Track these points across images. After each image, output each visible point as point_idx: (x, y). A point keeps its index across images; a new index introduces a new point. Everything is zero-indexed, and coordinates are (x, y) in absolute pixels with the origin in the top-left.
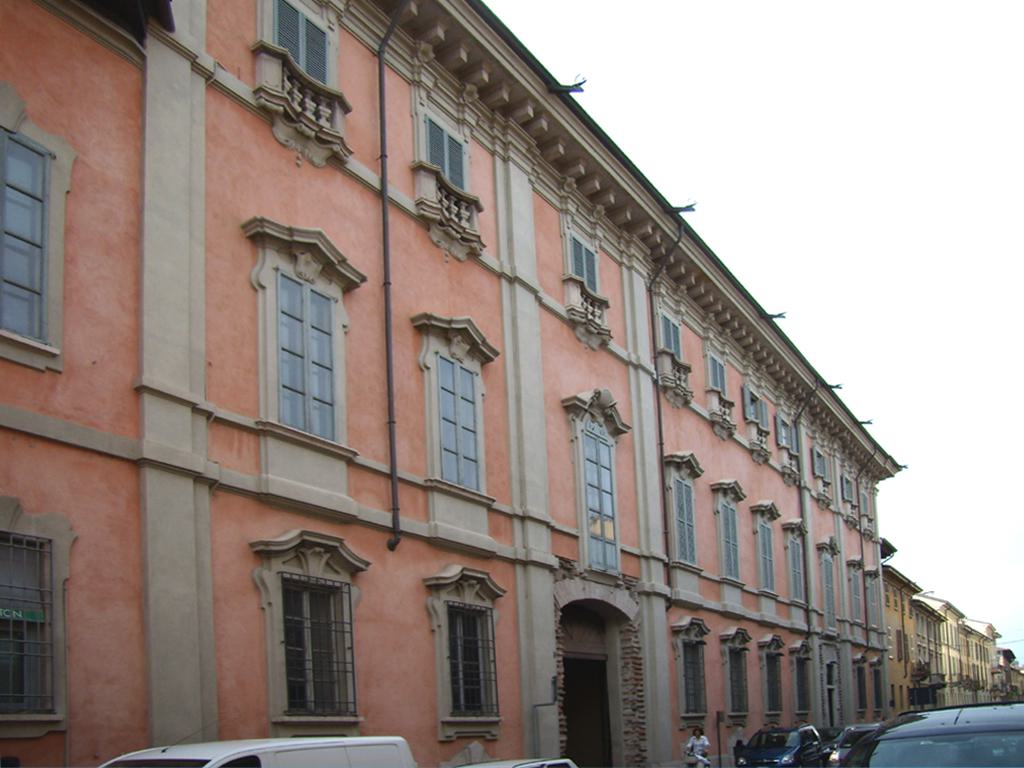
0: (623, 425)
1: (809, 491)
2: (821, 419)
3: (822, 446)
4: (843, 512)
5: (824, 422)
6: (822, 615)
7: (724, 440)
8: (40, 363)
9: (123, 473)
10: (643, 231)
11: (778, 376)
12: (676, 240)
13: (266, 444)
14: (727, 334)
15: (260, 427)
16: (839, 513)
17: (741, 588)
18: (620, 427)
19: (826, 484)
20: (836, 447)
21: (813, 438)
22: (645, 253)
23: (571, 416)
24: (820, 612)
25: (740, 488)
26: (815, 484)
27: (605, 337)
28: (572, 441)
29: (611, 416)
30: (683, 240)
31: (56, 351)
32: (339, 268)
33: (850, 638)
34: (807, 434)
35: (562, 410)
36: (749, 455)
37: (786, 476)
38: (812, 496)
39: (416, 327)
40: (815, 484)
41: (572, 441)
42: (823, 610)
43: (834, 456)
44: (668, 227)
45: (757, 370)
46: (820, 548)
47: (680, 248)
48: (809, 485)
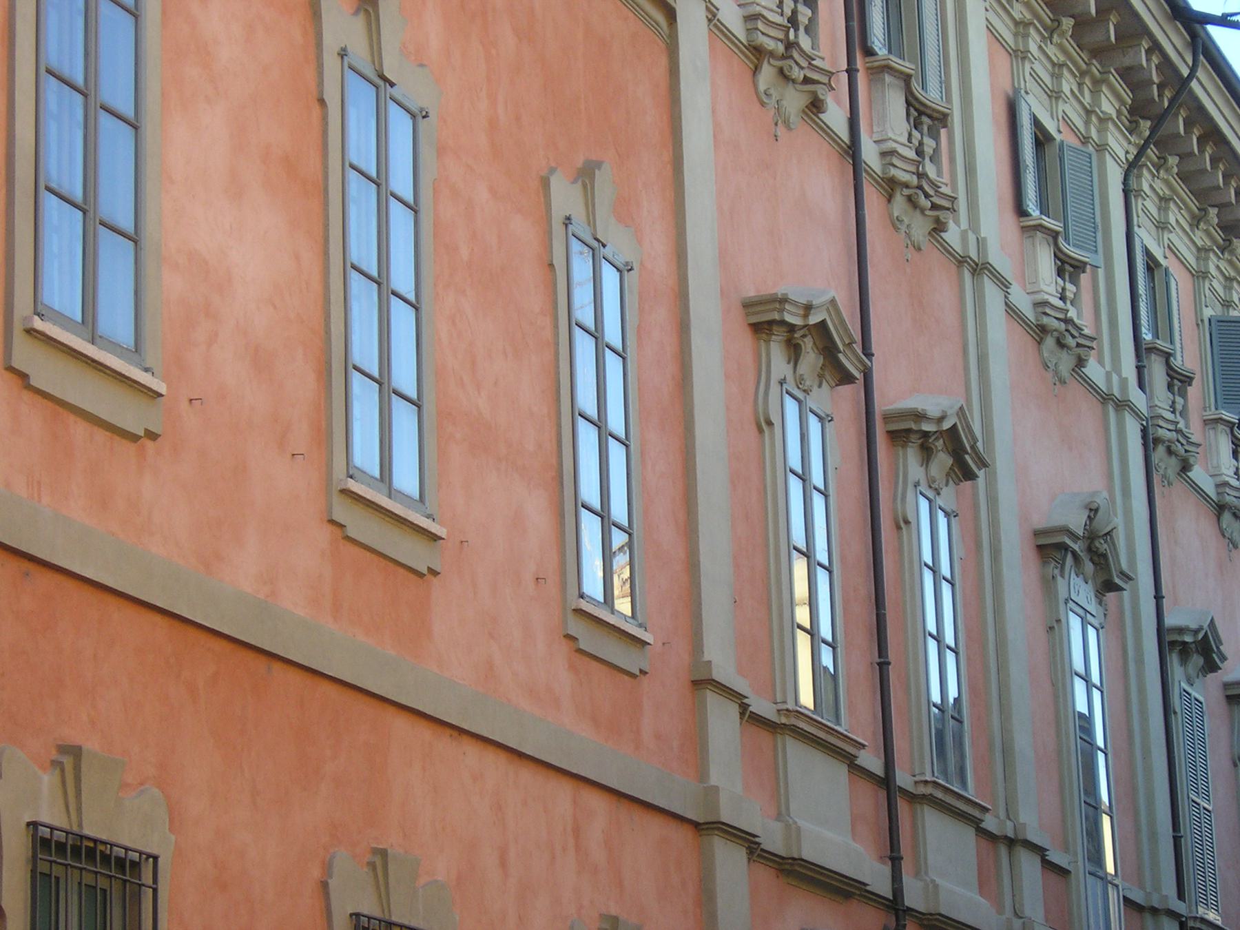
0: (1122, 573)
1: (1004, 284)
2: (1184, 157)
3: (1055, 95)
4: (1138, 398)
5: (1192, 167)
6: (1063, 872)
7: (1063, 382)
8: (131, 415)
9: (680, 836)
10: (1127, 61)
11: (1206, 183)
12: (1185, 72)
13: (922, 811)
14: (1208, 222)
15: (784, 720)
16: (1123, 405)
17: (976, 823)
18: (1117, 580)
19: (1068, 268)
20: (1108, 106)
21: (1019, 55)
22: (1122, 102)
23: (1052, 569)
24: (1056, 857)
25: (1219, 641)
26: (1026, 263)
27: (942, 215)
28: (1051, 628)
29: (1104, 556)
30: (1200, 73)
31: (161, 387)
32: (841, 356)
33: (752, 815)
34: (990, 28)
35: (1032, 554)
36: (954, 268)
37: (1050, 342)
38: (1011, 310)
39: (1040, 548)
40: (1026, 263)
41: (1051, 628)
42: (1066, 848)
43: (1102, 148)
44: (1172, 41)
45: (1196, 221)
46: (1050, 548)
47: (1191, 92)
48: (998, 258)
